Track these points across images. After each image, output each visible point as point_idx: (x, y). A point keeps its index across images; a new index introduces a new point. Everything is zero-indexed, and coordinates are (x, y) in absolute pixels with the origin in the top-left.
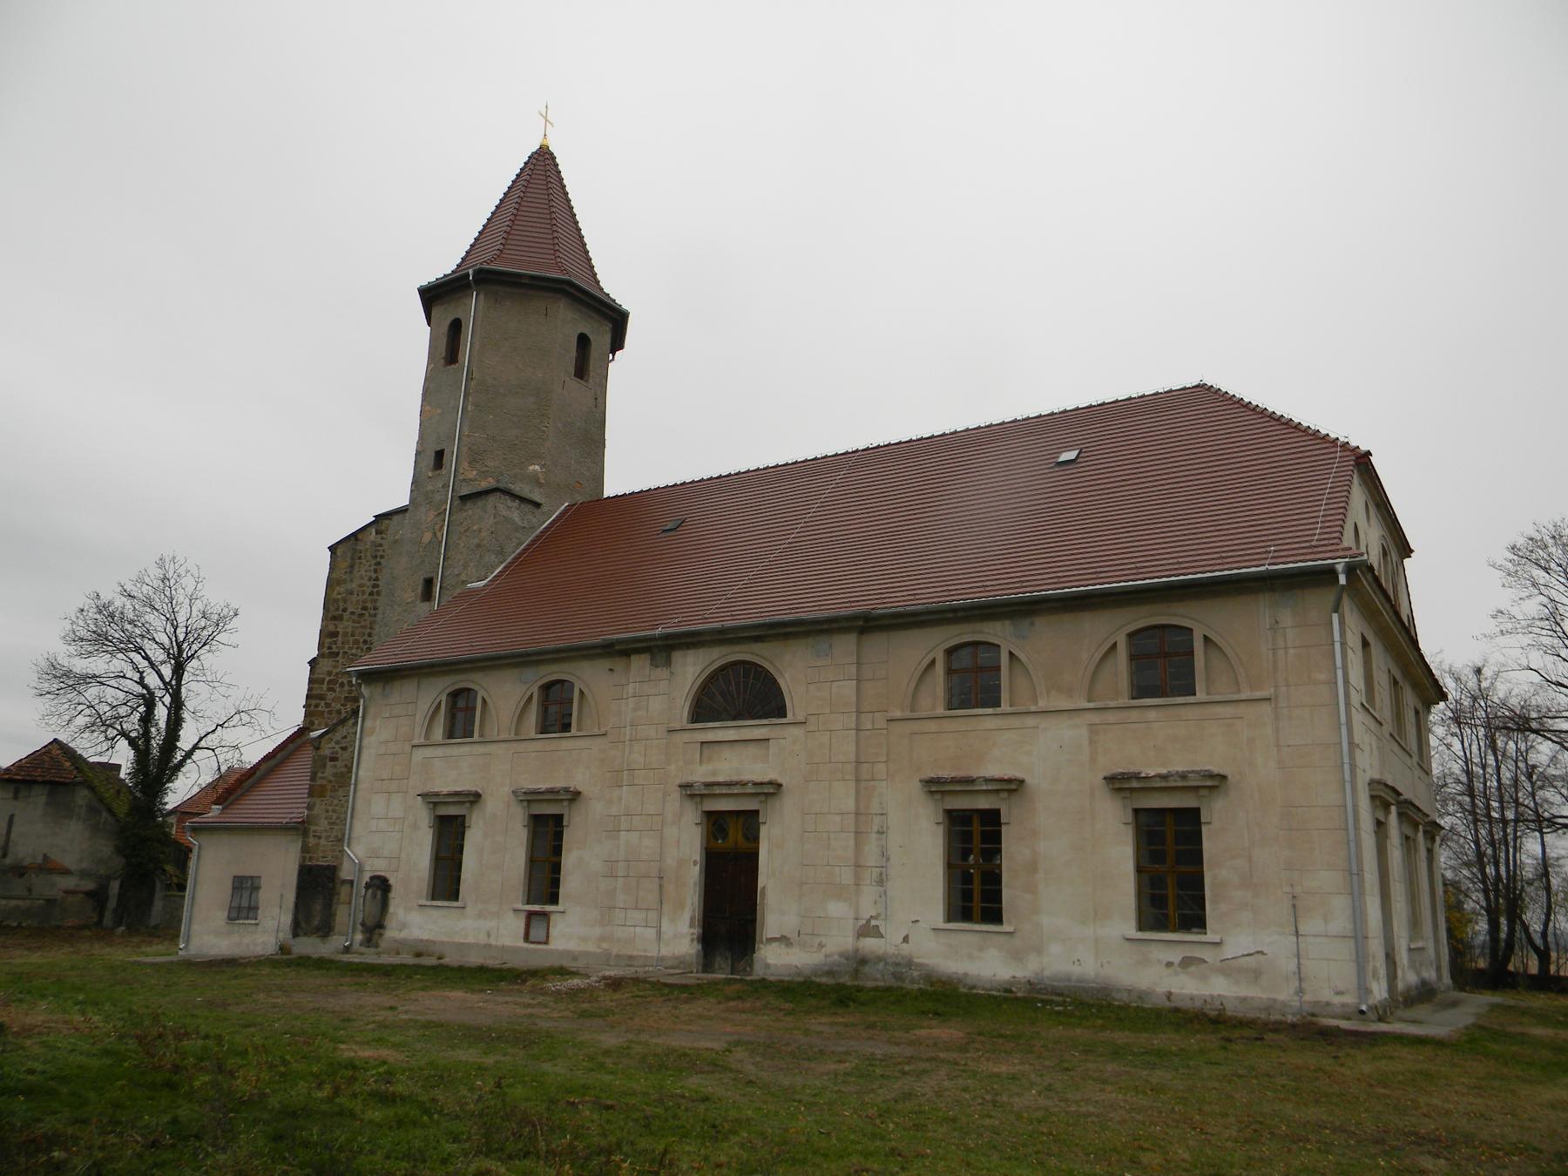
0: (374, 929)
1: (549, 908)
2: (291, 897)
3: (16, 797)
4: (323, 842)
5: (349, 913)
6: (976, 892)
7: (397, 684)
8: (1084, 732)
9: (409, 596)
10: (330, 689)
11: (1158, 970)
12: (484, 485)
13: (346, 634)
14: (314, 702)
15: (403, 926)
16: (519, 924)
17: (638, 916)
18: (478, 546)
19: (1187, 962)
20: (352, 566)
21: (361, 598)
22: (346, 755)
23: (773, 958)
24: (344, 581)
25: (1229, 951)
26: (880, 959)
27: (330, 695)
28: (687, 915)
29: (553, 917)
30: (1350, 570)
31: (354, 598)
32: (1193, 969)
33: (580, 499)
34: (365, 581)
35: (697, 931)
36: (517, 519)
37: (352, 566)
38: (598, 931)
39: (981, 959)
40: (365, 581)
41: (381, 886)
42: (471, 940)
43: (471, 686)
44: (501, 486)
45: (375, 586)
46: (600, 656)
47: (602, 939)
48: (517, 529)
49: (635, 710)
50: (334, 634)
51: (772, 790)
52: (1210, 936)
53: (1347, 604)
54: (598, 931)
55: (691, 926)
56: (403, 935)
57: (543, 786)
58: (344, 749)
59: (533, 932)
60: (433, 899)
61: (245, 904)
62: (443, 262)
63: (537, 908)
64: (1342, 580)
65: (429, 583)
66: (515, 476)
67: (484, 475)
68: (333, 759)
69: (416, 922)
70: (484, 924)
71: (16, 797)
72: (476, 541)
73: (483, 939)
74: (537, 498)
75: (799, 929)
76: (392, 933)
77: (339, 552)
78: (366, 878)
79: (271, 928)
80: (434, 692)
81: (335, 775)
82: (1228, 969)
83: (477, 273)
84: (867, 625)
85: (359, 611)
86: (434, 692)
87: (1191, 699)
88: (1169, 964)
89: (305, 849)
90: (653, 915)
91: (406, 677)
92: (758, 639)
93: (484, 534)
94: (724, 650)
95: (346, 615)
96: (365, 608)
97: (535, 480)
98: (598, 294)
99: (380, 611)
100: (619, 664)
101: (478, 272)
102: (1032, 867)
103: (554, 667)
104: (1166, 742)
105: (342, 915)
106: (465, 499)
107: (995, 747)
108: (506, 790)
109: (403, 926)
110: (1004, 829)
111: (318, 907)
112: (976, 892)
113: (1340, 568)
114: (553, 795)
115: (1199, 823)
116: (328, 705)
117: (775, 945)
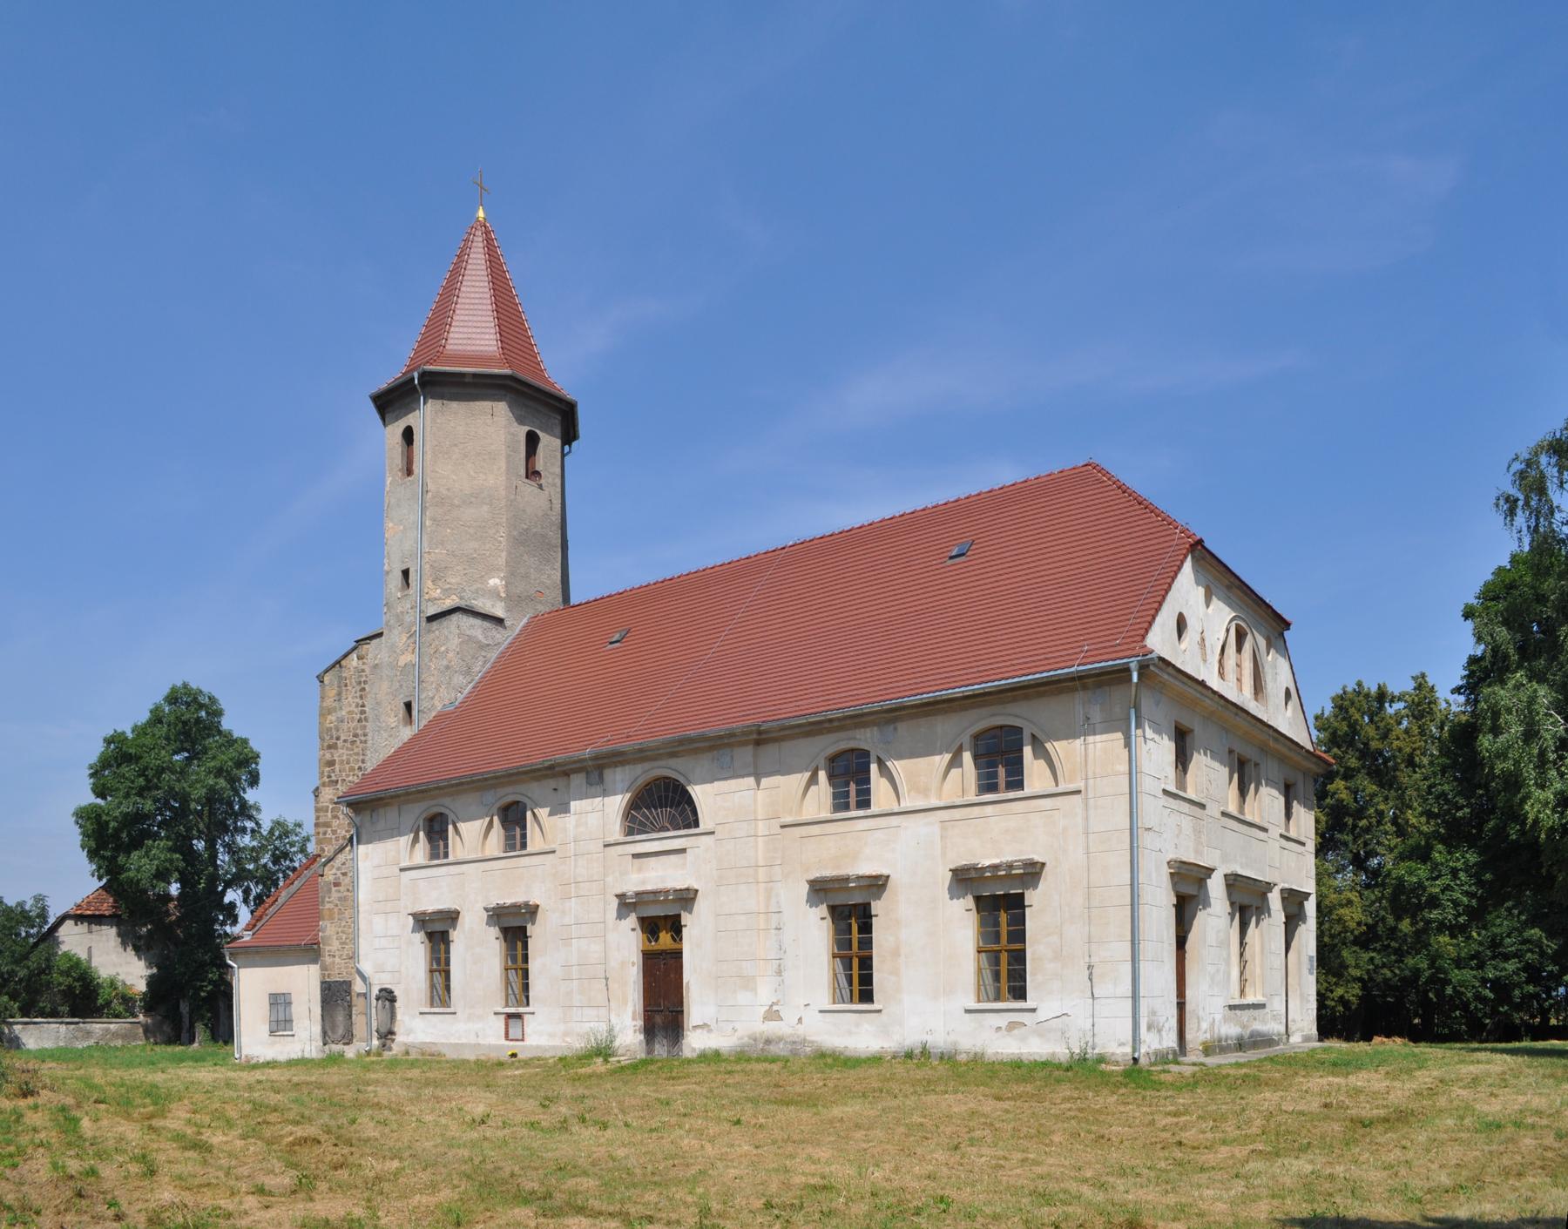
0: (387, 1035)
1: (521, 1010)
2: (317, 1010)
3: (90, 932)
4: (337, 960)
5: (365, 1021)
6: (858, 978)
7: (382, 811)
8: (936, 829)
9: (393, 721)
10: (336, 817)
11: (998, 1037)
12: (448, 603)
13: (342, 762)
14: (321, 830)
15: (409, 1032)
16: (500, 1022)
17: (592, 1012)
18: (448, 667)
19: (1012, 1026)
20: (339, 694)
21: (352, 725)
22: (347, 880)
23: (695, 1041)
24: (335, 710)
25: (1042, 1015)
26: (780, 1039)
27: (335, 823)
28: (630, 1009)
29: (526, 1017)
30: (1143, 668)
31: (345, 726)
32: (1016, 1032)
33: (542, 609)
34: (353, 708)
35: (640, 1023)
36: (481, 637)
37: (339, 694)
38: (562, 1027)
39: (859, 1034)
40: (353, 708)
41: (388, 996)
42: (464, 1041)
43: (442, 810)
44: (463, 604)
45: (363, 712)
46: (546, 777)
47: (566, 1034)
48: (482, 647)
49: (577, 826)
50: (331, 763)
51: (687, 898)
52: (1029, 1004)
53: (1147, 704)
54: (562, 1027)
55: (634, 1019)
56: (410, 1039)
57: (509, 902)
58: (344, 874)
59: (511, 1031)
60: (432, 1005)
61: (281, 1017)
62: (93, 758)
63: (512, 1010)
64: (1135, 678)
65: (408, 706)
66: (477, 591)
67: (447, 592)
68: (337, 884)
69: (418, 1029)
70: (471, 1027)
71: (90, 932)
72: (445, 663)
73: (473, 1040)
74: (500, 613)
75: (715, 1019)
76: (401, 1038)
77: (326, 679)
78: (375, 991)
79: (305, 1039)
80: (416, 812)
81: (340, 899)
82: (1041, 1030)
83: (423, 375)
84: (761, 738)
85: (351, 738)
86: (416, 812)
87: (1019, 794)
88: (999, 1028)
89: (324, 968)
90: (603, 1011)
91: (387, 805)
92: (673, 755)
93: (451, 655)
94: (647, 765)
95: (340, 743)
96: (356, 735)
97: (494, 593)
98: (547, 388)
99: (369, 738)
100: (560, 783)
101: (424, 375)
102: (896, 953)
103: (509, 789)
104: (999, 835)
105: (359, 1022)
106: (431, 619)
107: (860, 848)
108: (480, 906)
109: (409, 1032)
110: (1028, 910)
111: (340, 1018)
112: (858, 978)
113: (1133, 666)
114: (515, 909)
115: (1023, 907)
116: (334, 832)
117: (699, 1031)
